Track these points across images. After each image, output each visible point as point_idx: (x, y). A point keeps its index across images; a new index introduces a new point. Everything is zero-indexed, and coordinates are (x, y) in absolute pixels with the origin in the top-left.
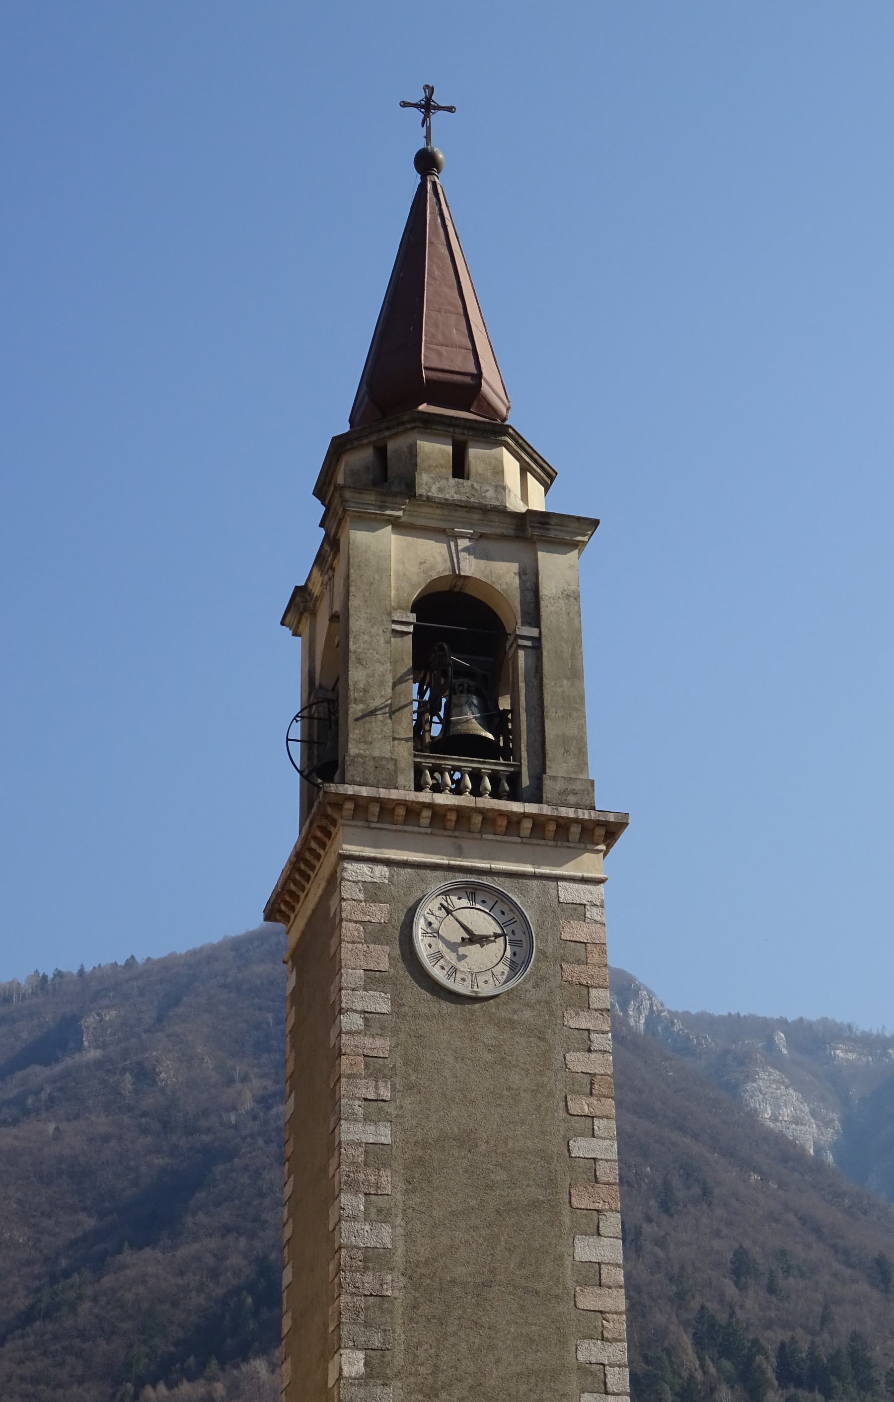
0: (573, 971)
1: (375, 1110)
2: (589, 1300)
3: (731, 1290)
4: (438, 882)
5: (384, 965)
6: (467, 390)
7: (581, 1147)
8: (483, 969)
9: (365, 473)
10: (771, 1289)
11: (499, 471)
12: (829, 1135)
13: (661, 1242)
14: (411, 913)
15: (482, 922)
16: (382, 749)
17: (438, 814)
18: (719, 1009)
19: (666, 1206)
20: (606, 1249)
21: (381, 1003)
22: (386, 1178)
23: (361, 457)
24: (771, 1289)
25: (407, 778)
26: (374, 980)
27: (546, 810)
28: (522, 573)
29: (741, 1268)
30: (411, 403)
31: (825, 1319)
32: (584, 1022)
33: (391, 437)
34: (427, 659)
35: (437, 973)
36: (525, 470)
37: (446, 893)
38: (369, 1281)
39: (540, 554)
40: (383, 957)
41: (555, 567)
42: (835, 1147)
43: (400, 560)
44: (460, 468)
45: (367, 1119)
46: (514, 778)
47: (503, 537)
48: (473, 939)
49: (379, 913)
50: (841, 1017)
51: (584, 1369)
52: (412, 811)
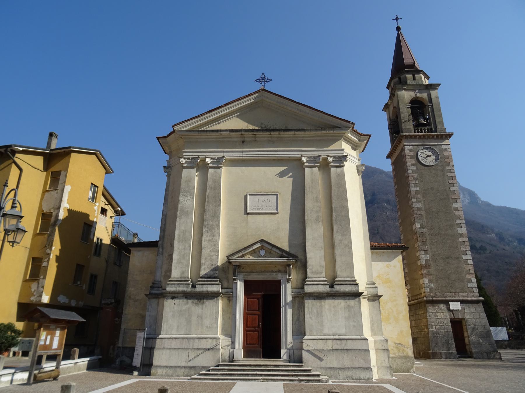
4: (421, 148)
8: (431, 161)
11: (421, 78)
14: (417, 153)
15: (429, 153)
16: (408, 127)
21: (414, 168)
26: (413, 164)
28: (428, 95)
30: (402, 69)
38: (419, 212)
40: (414, 161)
41: (433, 93)
43: (406, 96)
44: (414, 79)
45: (415, 187)
46: (431, 129)
47: (424, 89)
48: (428, 156)
49: (412, 154)
51: (457, 224)
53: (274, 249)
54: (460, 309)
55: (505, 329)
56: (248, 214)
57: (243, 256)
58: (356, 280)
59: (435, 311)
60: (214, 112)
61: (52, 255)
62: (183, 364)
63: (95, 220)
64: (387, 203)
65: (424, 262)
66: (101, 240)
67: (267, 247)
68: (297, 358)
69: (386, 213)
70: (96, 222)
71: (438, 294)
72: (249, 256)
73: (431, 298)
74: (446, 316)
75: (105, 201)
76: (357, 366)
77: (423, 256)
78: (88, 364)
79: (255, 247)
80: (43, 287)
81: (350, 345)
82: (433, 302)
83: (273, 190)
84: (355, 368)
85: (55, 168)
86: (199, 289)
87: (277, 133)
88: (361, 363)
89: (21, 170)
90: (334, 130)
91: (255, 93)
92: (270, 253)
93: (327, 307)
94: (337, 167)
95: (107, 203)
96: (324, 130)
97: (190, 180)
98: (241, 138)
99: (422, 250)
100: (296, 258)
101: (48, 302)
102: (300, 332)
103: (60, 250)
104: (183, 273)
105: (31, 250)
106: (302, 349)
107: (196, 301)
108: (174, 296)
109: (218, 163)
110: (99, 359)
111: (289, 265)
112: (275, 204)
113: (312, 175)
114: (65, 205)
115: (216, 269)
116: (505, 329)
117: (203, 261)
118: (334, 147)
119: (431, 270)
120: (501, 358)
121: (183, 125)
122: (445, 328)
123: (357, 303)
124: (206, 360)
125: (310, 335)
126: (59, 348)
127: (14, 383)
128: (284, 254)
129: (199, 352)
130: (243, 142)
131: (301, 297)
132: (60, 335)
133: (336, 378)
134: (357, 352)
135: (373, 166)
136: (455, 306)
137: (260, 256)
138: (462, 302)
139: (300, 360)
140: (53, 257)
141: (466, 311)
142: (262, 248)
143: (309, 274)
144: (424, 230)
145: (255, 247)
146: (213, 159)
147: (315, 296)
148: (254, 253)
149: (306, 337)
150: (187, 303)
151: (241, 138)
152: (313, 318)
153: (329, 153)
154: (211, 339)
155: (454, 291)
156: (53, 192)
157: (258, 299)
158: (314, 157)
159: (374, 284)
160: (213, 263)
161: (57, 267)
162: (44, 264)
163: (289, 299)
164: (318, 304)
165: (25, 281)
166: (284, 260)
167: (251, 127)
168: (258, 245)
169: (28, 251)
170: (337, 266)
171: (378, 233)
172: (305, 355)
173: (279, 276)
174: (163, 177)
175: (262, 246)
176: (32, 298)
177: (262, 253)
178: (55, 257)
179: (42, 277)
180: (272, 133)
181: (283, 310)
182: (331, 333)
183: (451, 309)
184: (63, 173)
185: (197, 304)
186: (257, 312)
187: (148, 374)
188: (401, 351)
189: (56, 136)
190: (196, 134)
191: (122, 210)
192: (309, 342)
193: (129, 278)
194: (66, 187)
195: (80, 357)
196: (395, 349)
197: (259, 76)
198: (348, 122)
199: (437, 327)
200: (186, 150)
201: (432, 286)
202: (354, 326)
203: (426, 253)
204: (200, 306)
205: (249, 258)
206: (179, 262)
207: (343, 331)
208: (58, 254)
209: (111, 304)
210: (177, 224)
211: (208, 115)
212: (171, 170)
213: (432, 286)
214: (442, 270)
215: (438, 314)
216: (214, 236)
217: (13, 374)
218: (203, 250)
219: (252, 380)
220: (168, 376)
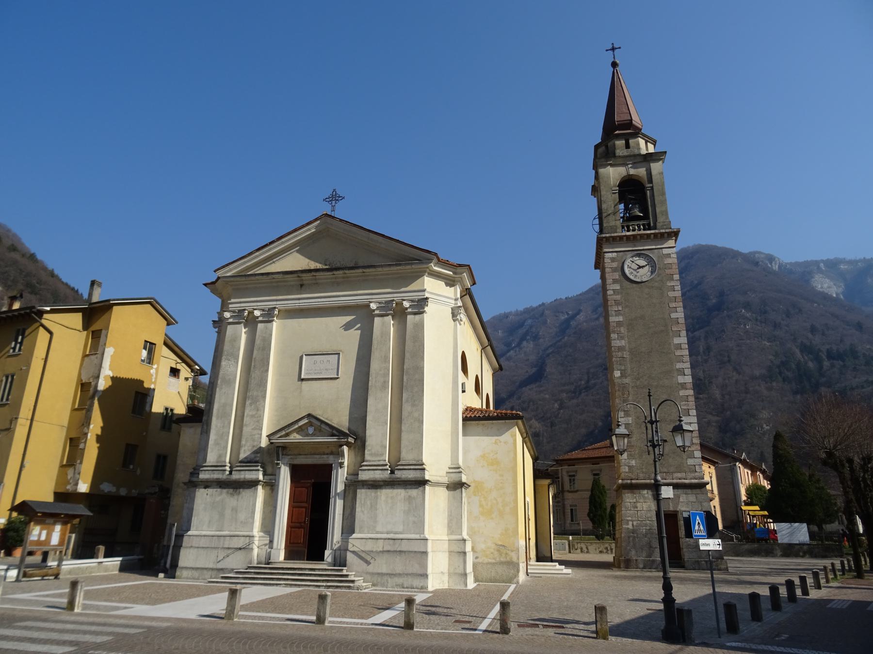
1: (618, 313)
2: (678, 353)
3: (810, 336)
4: (630, 254)
6: (629, 124)
7: (673, 315)
8: (644, 274)
9: (604, 154)
10: (823, 334)
11: (638, 144)
12: (840, 290)
13: (787, 326)
14: (623, 263)
15: (642, 262)
16: (612, 223)
17: (628, 237)
18: (801, 260)
19: (788, 316)
20: (683, 340)
21: (617, 287)
22: (622, 329)
23: (602, 150)
24: (823, 334)
25: (620, 230)
26: (615, 281)
27: (657, 231)
29: (813, 330)
30: (617, 129)
31: (841, 341)
32: (672, 284)
33: (52, 311)
34: (622, 198)
35: (632, 277)
36: (646, 142)
38: (620, 354)
39: (652, 164)
40: (617, 275)
41: (656, 167)
42: (843, 293)
43: (613, 174)
46: (649, 224)
48: (640, 267)
49: (615, 265)
50: (841, 256)
52: (621, 238)
53: (323, 426)
54: (671, 496)
55: (805, 525)
56: (303, 380)
57: (287, 435)
58: (423, 464)
60: (283, 240)
61: (89, 435)
62: (211, 566)
63: (152, 387)
64: (745, 308)
66: (172, 410)
67: (314, 423)
68: (340, 561)
69: (745, 325)
70: (154, 390)
71: (641, 475)
72: (295, 434)
73: (629, 481)
75: (175, 358)
76: (410, 572)
78: (121, 564)
79: (301, 423)
80: (79, 474)
81: (404, 546)
82: (633, 488)
83: (335, 348)
84: (407, 574)
85: (95, 327)
86: (236, 476)
87: (341, 272)
88: (416, 569)
89: (51, 333)
90: (412, 264)
91: (316, 220)
92: (320, 431)
93: (383, 498)
94: (415, 314)
95: (179, 361)
96: (400, 265)
97: (236, 339)
98: (299, 281)
100: (356, 436)
102: (349, 529)
103: (102, 428)
104: (220, 456)
105: (69, 429)
106: (347, 550)
107: (231, 490)
108: (207, 484)
109: (269, 315)
110: (140, 560)
111: (341, 446)
112: (336, 367)
113: (386, 328)
114: (107, 372)
115: (260, 450)
116: (805, 525)
117: (243, 442)
118: (413, 286)
119: (634, 439)
120: (727, 569)
121: (227, 269)
122: (646, 525)
123: (420, 493)
124: (236, 562)
125: (360, 533)
127: (8, 580)
128: (335, 432)
129: (230, 551)
130: (302, 285)
131: (354, 485)
132: (61, 530)
133: (383, 585)
134: (412, 555)
135: (720, 245)
137: (308, 435)
138: (676, 486)
139: (344, 564)
140: (91, 437)
141: (681, 500)
142: (310, 424)
143: (367, 457)
144: (627, 381)
145: (301, 423)
146: (263, 310)
148: (300, 430)
149: (354, 536)
150: (221, 494)
151: (299, 281)
152: (366, 512)
153: (405, 297)
154: (244, 536)
155: (666, 470)
156: (93, 357)
157: (307, 488)
158: (386, 302)
159: (459, 468)
160: (255, 443)
161: (99, 448)
162: (81, 446)
163: (340, 487)
164: (373, 494)
165: (62, 466)
166: (334, 439)
167: (313, 265)
168: (305, 421)
169: (65, 430)
170: (402, 446)
171: (729, 361)
172: (350, 557)
173: (331, 459)
174: (213, 333)
175: (310, 422)
176: (69, 487)
177: (311, 430)
178: (94, 438)
179: (79, 461)
180: (335, 272)
181: (332, 501)
182: (385, 530)
184: (103, 332)
185: (232, 495)
187: (174, 577)
188: (504, 555)
189: (100, 285)
190: (244, 279)
191: (201, 369)
192: (356, 542)
193: (179, 462)
194: (106, 350)
195: (105, 557)
196: (496, 553)
197: (328, 194)
199: (635, 523)
200: (233, 300)
201: (633, 463)
202: (414, 522)
203: (627, 414)
204: (236, 497)
205: (295, 438)
206: (217, 443)
207: (400, 528)
208: (99, 433)
209: (155, 493)
210: (217, 396)
211: (257, 253)
212: (220, 324)
213: (633, 463)
215: (638, 505)
216: (258, 410)
217: (7, 570)
218: (244, 428)
219: (273, 585)
220: (194, 579)
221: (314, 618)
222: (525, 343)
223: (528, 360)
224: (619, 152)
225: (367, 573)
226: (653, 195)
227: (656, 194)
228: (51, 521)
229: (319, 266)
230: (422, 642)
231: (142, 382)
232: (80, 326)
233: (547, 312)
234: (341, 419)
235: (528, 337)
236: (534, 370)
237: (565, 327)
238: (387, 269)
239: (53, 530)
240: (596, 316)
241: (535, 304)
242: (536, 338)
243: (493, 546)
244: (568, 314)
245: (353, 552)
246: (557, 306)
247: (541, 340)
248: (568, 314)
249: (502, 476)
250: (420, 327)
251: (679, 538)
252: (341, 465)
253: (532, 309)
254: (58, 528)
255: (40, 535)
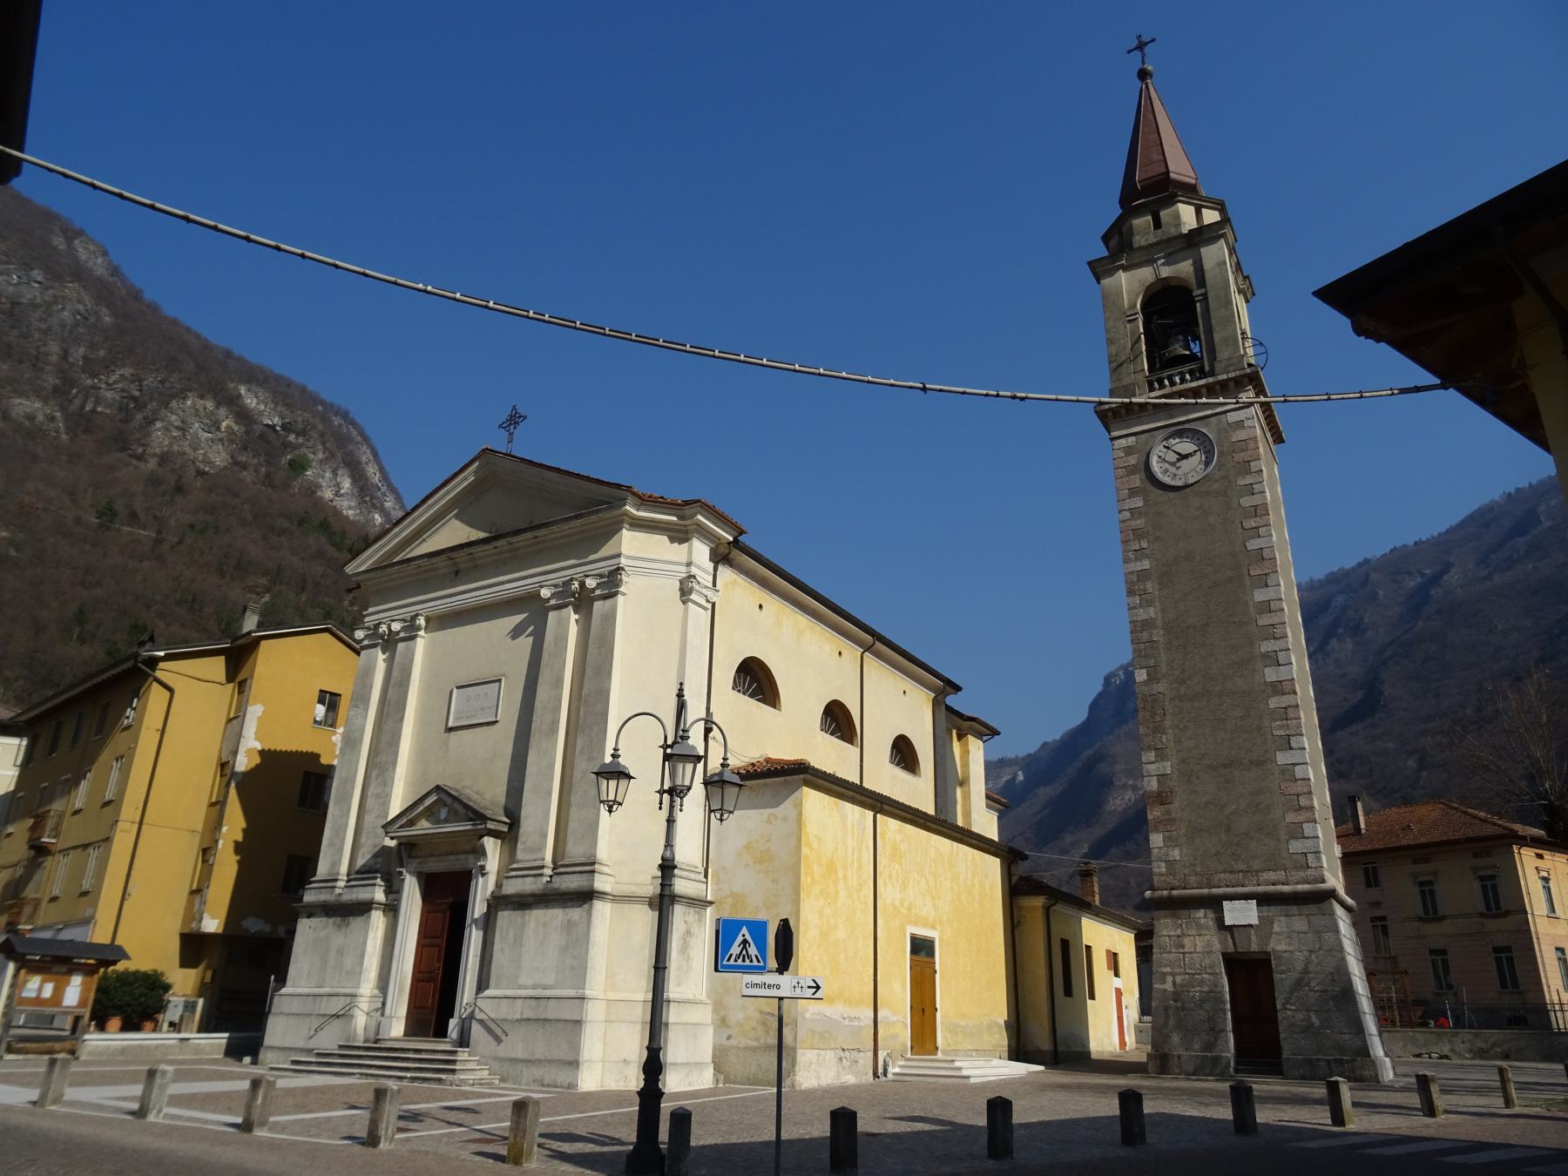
0: (1239, 457)
4: (1160, 435)
5: (1138, 484)
8: (1192, 469)
9: (1121, 245)
15: (1186, 446)
22: (1149, 586)
23: (1114, 242)
28: (1194, 264)
33: (168, 658)
35: (1167, 480)
37: (1167, 439)
43: (1129, 284)
44: (1157, 224)
45: (1137, 559)
47: (1181, 250)
49: (1132, 460)
51: (1265, 656)
54: (1254, 921)
56: (450, 730)
57: (411, 823)
59: (1179, 932)
60: (430, 502)
65: (1153, 785)
73: (1165, 893)
74: (1209, 944)
77: (1152, 767)
81: (552, 1011)
84: (551, 1061)
85: (240, 678)
88: (562, 1053)
89: (170, 690)
90: (598, 511)
93: (532, 925)
94: (605, 597)
99: (1149, 748)
101: (220, 931)
103: (244, 831)
109: (411, 630)
119: (1176, 805)
125: (497, 987)
126: (82, 1003)
130: (457, 572)
132: (83, 984)
136: (1240, 913)
138: (1264, 900)
141: (1276, 928)
143: (520, 855)
144: (1161, 687)
147: (513, 903)
148: (430, 813)
151: (456, 565)
155: (1243, 867)
161: (239, 862)
168: (433, 798)
169: (197, 838)
182: (530, 983)
183: (1228, 922)
185: (339, 927)
186: (438, 941)
190: (379, 573)
195: (199, 1031)
196: (760, 1027)
197: (504, 416)
198: (618, 486)
199: (1178, 979)
200: (371, 610)
201: (1176, 854)
202: (573, 968)
203: (1161, 755)
205: (424, 827)
206: (331, 845)
207: (551, 980)
208: (240, 838)
213: (1176, 854)
214: (1206, 804)
215: (1186, 941)
221: (239, 1120)
222: (1334, 643)
223: (1344, 675)
224: (1139, 241)
225: (497, 1059)
226: (1207, 311)
227: (1212, 305)
228: (65, 968)
229: (482, 535)
230: (160, 1144)
231: (318, 756)
232: (222, 677)
233: (1374, 576)
234: (489, 792)
235: (1341, 631)
236: (1360, 694)
237: (1418, 601)
238: (565, 526)
239: (68, 983)
240: (1486, 572)
241: (1349, 563)
242: (1357, 629)
243: (756, 1015)
244: (1422, 575)
245: (481, 1022)
246: (1398, 562)
247: (1370, 633)
248: (1422, 575)
249: (775, 881)
250: (610, 619)
251: (1276, 1011)
252: (482, 871)
253: (1345, 574)
254: (77, 980)
255: (40, 989)
